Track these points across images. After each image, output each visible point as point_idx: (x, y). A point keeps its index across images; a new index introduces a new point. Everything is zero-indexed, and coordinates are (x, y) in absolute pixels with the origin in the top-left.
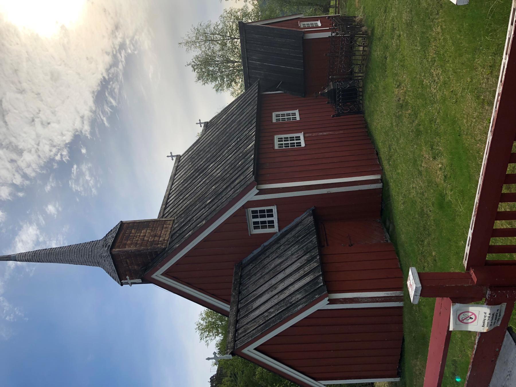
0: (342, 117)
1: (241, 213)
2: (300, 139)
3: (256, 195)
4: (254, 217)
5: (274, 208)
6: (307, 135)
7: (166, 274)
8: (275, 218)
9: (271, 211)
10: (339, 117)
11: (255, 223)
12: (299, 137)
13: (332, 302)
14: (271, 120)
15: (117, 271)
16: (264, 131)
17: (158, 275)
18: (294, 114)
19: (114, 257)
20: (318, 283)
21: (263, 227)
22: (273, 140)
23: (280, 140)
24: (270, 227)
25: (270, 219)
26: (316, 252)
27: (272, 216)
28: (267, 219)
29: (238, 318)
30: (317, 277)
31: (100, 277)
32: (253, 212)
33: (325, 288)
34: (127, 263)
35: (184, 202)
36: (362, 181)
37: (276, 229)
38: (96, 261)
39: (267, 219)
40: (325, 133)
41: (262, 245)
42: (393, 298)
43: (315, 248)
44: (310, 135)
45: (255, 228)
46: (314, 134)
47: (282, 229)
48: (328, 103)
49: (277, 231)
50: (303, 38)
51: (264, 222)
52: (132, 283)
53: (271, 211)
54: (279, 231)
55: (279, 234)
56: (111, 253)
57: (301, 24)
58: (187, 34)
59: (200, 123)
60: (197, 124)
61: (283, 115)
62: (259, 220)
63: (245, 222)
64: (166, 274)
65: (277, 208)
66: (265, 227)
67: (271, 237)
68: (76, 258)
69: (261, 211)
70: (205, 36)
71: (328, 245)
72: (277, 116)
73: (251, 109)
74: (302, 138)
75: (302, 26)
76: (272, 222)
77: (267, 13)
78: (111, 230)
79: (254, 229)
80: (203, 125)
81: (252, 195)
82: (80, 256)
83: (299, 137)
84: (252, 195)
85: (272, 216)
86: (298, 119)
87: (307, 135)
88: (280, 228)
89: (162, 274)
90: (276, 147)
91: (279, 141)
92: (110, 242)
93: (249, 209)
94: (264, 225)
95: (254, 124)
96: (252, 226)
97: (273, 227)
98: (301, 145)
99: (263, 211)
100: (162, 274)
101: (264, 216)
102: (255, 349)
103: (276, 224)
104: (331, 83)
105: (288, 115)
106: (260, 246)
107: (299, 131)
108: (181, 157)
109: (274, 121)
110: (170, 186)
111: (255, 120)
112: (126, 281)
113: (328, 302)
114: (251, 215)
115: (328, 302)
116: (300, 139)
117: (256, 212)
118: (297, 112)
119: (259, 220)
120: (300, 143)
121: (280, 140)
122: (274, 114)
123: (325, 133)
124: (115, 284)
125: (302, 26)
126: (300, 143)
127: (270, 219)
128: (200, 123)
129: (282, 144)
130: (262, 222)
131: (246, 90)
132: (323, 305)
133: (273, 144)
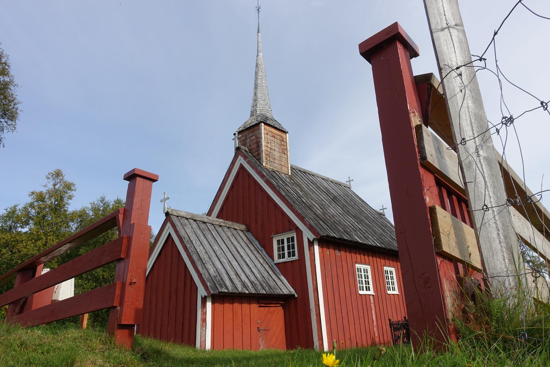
1: (292, 227)
4: (288, 239)
5: (296, 257)
6: (371, 298)
7: (242, 167)
8: (287, 259)
9: (294, 255)
11: (283, 241)
17: (241, 160)
19: (258, 125)
20: (222, 287)
21: (279, 248)
22: (365, 264)
24: (279, 255)
29: (198, 222)
30: (227, 288)
32: (293, 238)
33: (216, 292)
34: (252, 136)
37: (277, 260)
40: (374, 317)
43: (256, 290)
44: (372, 301)
45: (278, 241)
46: (373, 305)
47: (278, 267)
49: (275, 262)
51: (283, 250)
53: (294, 255)
54: (275, 264)
55: (273, 264)
56: (260, 122)
59: (350, 181)
63: (284, 231)
64: (242, 167)
66: (279, 251)
67: (267, 253)
69: (293, 245)
72: (391, 273)
74: (368, 293)
76: (284, 257)
80: (382, 211)
81: (308, 235)
83: (369, 290)
84: (308, 235)
89: (241, 164)
93: (295, 234)
95: (379, 245)
96: (280, 238)
98: (360, 290)
99: (293, 248)
100: (241, 164)
101: (289, 249)
102: (170, 234)
103: (282, 260)
105: (393, 283)
111: (384, 246)
114: (290, 236)
117: (293, 241)
120: (363, 290)
123: (374, 317)
124: (236, 130)
128: (350, 181)
130: (283, 248)
133: (361, 263)
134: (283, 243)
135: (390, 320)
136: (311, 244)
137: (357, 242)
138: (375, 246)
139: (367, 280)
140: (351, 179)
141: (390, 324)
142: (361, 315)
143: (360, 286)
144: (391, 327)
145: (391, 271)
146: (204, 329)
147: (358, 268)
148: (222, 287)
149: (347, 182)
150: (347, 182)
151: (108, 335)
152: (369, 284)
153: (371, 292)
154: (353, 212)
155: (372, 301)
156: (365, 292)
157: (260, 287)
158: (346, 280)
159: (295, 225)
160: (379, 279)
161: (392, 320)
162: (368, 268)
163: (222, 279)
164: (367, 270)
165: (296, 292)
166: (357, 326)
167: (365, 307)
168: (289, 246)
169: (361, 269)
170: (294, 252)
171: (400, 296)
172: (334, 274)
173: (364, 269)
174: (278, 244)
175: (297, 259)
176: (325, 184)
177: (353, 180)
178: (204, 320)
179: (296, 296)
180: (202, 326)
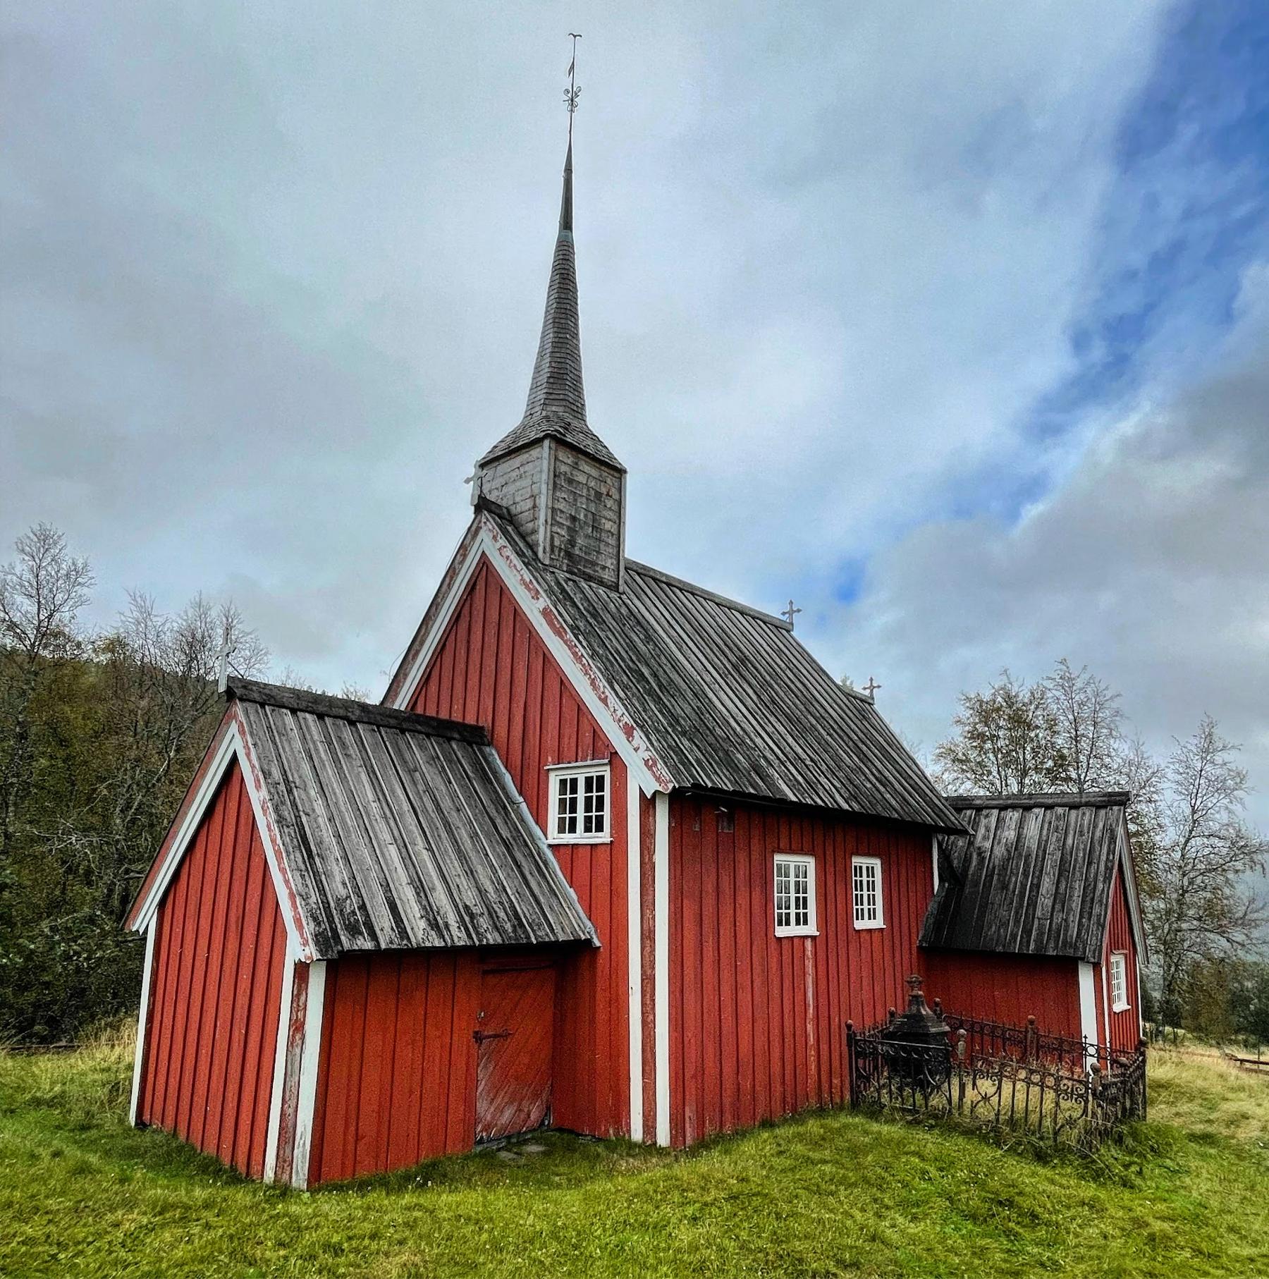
0: (845, 1049)
1: (599, 746)
2: (798, 923)
4: (589, 781)
5: (605, 837)
6: (809, 943)
8: (579, 837)
10: (844, 1041)
11: (574, 782)
13: (302, 971)
14: (858, 854)
16: (833, 831)
18: (873, 914)
20: (354, 930)
25: (580, 825)
26: (459, 937)
28: (580, 815)
32: (601, 779)
35: (851, 744)
36: (650, 1096)
37: (555, 837)
39: (580, 815)
41: (521, 799)
42: (288, 1151)
44: (809, 953)
45: (563, 782)
48: (892, 1014)
50: (1082, 959)
53: (600, 828)
54: (550, 846)
57: (1118, 960)
58: (1097, 680)
60: (791, 603)
61: (871, 886)
62: (581, 795)
66: (562, 809)
69: (600, 800)
70: (1092, 718)
71: (486, 973)
72: (871, 872)
73: (891, 805)
75: (1113, 959)
76: (573, 829)
80: (867, 692)
83: (806, 923)
86: (859, 925)
87: (809, 943)
88: (554, 848)
94: (569, 806)
95: (846, 806)
97: (561, 830)
98: (780, 924)
99: (600, 807)
101: (588, 808)
103: (568, 838)
105: (872, 900)
106: (521, 794)
108: (788, 631)
109: (857, 861)
111: (856, 807)
114: (594, 772)
117: (601, 788)
118: (878, 923)
119: (581, 795)
120: (788, 923)
122: (876, 863)
125: (1113, 959)
127: (580, 825)
128: (791, 613)
129: (787, 875)
131: (946, 799)
132: (298, 947)
133: (791, 851)
134: (574, 790)
136: (648, 804)
137: (784, 802)
138: (834, 809)
139: (801, 911)
142: (776, 992)
143: (780, 915)
144: (849, 1046)
145: (869, 868)
146: (298, 1051)
147: (779, 867)
148: (354, 930)
149: (784, 614)
150: (784, 614)
152: (805, 907)
153: (811, 929)
154: (788, 701)
155: (809, 953)
156: (792, 930)
157: (484, 923)
159: (608, 745)
160: (836, 894)
163: (363, 907)
166: (760, 1025)
167: (787, 971)
168: (588, 800)
170: (600, 820)
173: (796, 870)
174: (563, 791)
175: (608, 840)
176: (722, 619)
177: (799, 611)
178: (298, 1026)
180: (291, 1043)
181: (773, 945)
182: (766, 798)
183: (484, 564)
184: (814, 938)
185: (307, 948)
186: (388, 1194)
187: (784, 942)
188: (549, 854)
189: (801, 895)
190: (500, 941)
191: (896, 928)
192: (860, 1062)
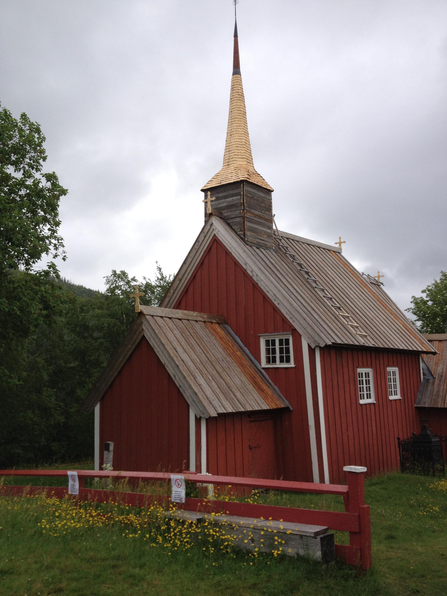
2: (367, 398)
3: (309, 345)
4: (281, 341)
5: (292, 364)
6: (372, 407)
8: (278, 365)
10: (397, 445)
11: (274, 342)
12: (370, 398)
15: (219, 186)
18: (396, 394)
21: (268, 351)
22: (367, 367)
23: (367, 375)
25: (278, 360)
27: (282, 361)
28: (278, 355)
31: (208, 165)
32: (287, 341)
38: (230, 163)
39: (278, 355)
45: (267, 342)
47: (266, 372)
52: (206, 203)
53: (288, 361)
59: (340, 243)
60: (340, 238)
63: (276, 330)
65: (292, 368)
68: (234, 140)
71: (251, 422)
76: (274, 361)
77: (276, 591)
78: (259, 174)
79: (266, 340)
80: (337, 246)
82: (238, 145)
83: (370, 398)
85: (282, 361)
90: (359, 370)
91: (365, 373)
92: (253, 180)
94: (271, 351)
97: (268, 362)
98: (361, 399)
104: (438, 439)
107: (377, 398)
108: (339, 253)
110: (307, 242)
112: (209, 196)
113: (198, 417)
114: (284, 337)
115: (198, 417)
116: (367, 398)
118: (398, 397)
120: (364, 399)
121: (367, 375)
126: (364, 399)
127: (278, 360)
128: (379, 277)
130: (274, 351)
133: (363, 367)
135: (398, 439)
139: (368, 392)
140: (342, 241)
141: (399, 443)
144: (399, 447)
147: (359, 373)
149: (336, 243)
150: (336, 243)
151: (309, 582)
158: (347, 388)
161: (401, 439)
162: (369, 370)
164: (368, 373)
165: (290, 404)
169: (362, 373)
171: (402, 401)
172: (335, 383)
177: (344, 242)
179: (291, 409)
181: (359, 408)
182: (357, 345)
183: (215, 241)
184: (374, 404)
185: (425, 401)
186: (414, 434)
187: (363, 406)
188: (263, 371)
189: (368, 386)
190: (269, 408)
191: (406, 399)
192: (404, 452)
